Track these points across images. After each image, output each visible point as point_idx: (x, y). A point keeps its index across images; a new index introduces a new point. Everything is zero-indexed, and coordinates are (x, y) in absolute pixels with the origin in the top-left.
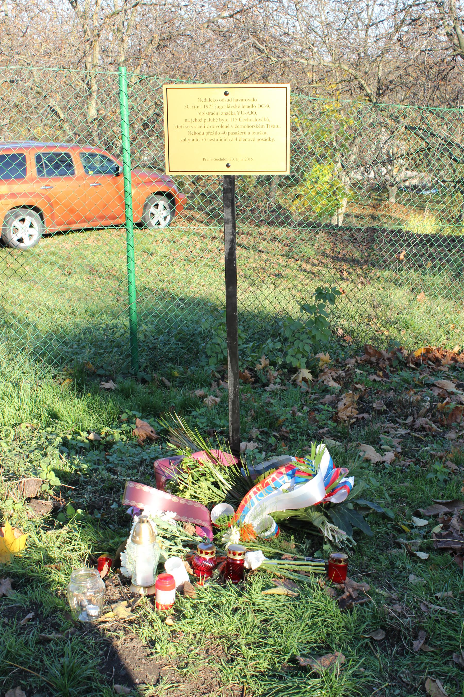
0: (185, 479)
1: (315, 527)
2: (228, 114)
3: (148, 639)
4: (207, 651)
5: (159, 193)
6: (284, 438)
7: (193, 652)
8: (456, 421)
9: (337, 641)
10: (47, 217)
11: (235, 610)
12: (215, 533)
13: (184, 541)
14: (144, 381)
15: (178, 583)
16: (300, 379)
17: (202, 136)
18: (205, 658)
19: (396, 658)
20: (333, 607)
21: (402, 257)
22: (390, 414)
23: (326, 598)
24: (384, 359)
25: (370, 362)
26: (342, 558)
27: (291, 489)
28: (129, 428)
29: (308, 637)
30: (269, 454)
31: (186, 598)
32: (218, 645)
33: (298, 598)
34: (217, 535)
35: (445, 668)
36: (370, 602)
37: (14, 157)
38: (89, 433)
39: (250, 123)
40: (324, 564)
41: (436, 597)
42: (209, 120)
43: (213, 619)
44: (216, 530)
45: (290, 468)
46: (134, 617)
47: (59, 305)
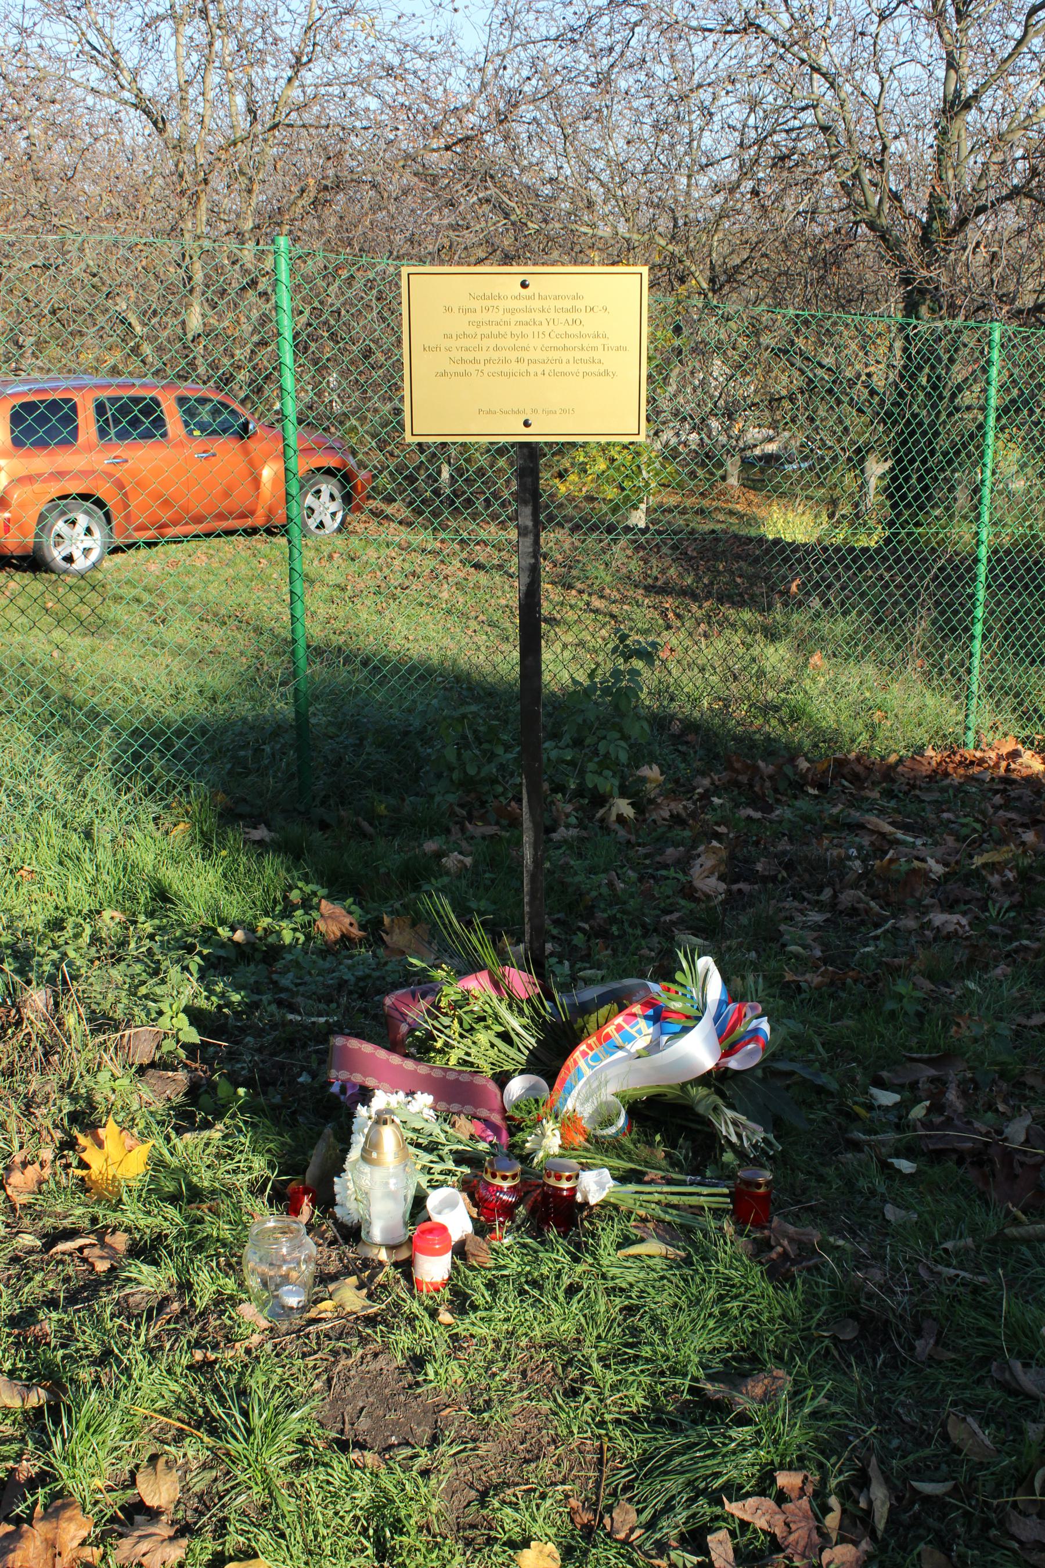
0: (446, 1027)
1: (698, 1115)
2: (527, 324)
3: (407, 1354)
4: (524, 1373)
5: (329, 472)
6: (602, 933)
7: (498, 1378)
8: (913, 896)
9: (771, 1346)
10: (117, 519)
11: (572, 1290)
12: (512, 1135)
13: (457, 1152)
14: (324, 826)
15: (456, 1236)
16: (613, 817)
17: (477, 366)
18: (521, 1390)
19: (884, 1375)
20: (756, 1276)
21: (794, 588)
22: (791, 883)
23: (740, 1260)
24: (761, 778)
25: (737, 784)
26: (761, 1180)
27: (654, 1047)
28: (307, 918)
29: (714, 1340)
30: (578, 966)
31: (472, 1268)
32: (544, 1362)
33: (688, 1261)
34: (516, 1139)
35: (979, 1391)
36: (825, 1264)
37: (54, 406)
38: (233, 929)
39: (570, 342)
40: (726, 1191)
41: (946, 1250)
42: (490, 336)
43: (531, 1311)
44: (514, 1127)
45: (650, 1003)
46: (376, 1308)
47: (153, 683)
